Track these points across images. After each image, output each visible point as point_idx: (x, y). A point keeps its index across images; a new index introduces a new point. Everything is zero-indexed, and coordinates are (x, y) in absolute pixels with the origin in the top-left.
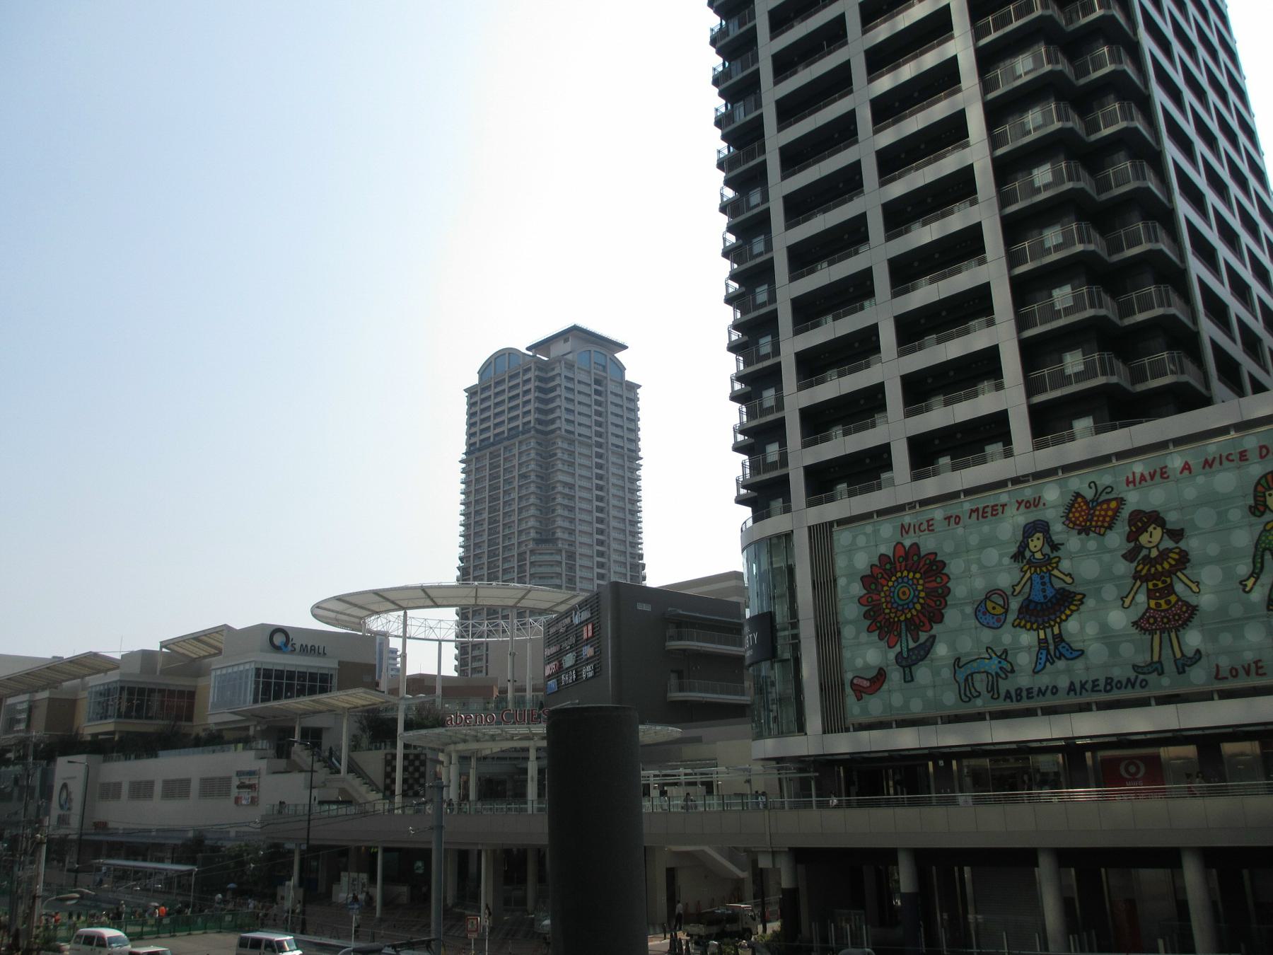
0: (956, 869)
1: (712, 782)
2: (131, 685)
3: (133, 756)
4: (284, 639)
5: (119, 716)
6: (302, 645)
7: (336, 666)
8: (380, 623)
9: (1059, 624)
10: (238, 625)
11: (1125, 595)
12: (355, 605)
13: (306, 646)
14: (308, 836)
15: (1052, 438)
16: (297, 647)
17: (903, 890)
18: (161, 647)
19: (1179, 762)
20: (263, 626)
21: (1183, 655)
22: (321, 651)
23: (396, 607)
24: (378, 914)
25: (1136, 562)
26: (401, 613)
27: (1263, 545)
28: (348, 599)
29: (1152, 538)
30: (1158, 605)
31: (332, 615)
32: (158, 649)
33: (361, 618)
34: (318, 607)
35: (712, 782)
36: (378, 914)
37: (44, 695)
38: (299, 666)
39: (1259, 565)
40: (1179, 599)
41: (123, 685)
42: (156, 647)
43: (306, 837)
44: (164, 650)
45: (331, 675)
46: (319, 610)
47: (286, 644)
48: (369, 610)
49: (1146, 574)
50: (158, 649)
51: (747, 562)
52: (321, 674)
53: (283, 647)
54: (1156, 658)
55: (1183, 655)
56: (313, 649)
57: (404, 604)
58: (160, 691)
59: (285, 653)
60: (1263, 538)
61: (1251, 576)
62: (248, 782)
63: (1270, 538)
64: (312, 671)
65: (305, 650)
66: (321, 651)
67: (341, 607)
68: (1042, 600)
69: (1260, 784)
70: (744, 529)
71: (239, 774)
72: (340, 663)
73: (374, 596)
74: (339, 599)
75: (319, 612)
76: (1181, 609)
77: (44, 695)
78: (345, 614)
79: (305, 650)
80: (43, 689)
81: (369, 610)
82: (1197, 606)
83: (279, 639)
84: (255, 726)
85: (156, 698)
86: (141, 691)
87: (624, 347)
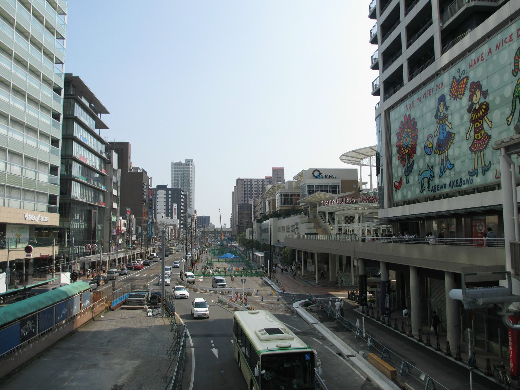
0: (425, 278)
2: (284, 193)
6: (326, 175)
8: (366, 161)
9: (447, 150)
10: (306, 170)
11: (467, 133)
12: (361, 154)
13: (328, 175)
15: (447, 47)
16: (324, 176)
18: (294, 179)
19: (491, 224)
20: (310, 169)
21: (485, 165)
22: (334, 177)
24: (317, 282)
25: (471, 113)
26: (369, 158)
27: (516, 94)
29: (477, 98)
30: (478, 136)
31: (349, 161)
32: (293, 180)
33: (358, 161)
34: (344, 155)
36: (317, 282)
38: (333, 183)
39: (514, 107)
40: (485, 133)
44: (295, 180)
45: (339, 186)
47: (319, 175)
48: (366, 155)
49: (474, 119)
50: (293, 180)
52: (334, 185)
53: (318, 177)
54: (476, 168)
55: (485, 165)
56: (330, 176)
57: (369, 154)
58: (295, 195)
59: (319, 179)
60: (516, 90)
61: (511, 114)
63: (519, 89)
64: (334, 184)
65: (327, 177)
66: (334, 177)
67: (354, 154)
68: (443, 139)
69: (462, 240)
72: (341, 181)
73: (370, 149)
74: (354, 151)
75: (343, 158)
76: (485, 138)
79: (327, 177)
81: (366, 155)
82: (491, 136)
83: (316, 174)
86: (288, 195)
87: (106, 112)
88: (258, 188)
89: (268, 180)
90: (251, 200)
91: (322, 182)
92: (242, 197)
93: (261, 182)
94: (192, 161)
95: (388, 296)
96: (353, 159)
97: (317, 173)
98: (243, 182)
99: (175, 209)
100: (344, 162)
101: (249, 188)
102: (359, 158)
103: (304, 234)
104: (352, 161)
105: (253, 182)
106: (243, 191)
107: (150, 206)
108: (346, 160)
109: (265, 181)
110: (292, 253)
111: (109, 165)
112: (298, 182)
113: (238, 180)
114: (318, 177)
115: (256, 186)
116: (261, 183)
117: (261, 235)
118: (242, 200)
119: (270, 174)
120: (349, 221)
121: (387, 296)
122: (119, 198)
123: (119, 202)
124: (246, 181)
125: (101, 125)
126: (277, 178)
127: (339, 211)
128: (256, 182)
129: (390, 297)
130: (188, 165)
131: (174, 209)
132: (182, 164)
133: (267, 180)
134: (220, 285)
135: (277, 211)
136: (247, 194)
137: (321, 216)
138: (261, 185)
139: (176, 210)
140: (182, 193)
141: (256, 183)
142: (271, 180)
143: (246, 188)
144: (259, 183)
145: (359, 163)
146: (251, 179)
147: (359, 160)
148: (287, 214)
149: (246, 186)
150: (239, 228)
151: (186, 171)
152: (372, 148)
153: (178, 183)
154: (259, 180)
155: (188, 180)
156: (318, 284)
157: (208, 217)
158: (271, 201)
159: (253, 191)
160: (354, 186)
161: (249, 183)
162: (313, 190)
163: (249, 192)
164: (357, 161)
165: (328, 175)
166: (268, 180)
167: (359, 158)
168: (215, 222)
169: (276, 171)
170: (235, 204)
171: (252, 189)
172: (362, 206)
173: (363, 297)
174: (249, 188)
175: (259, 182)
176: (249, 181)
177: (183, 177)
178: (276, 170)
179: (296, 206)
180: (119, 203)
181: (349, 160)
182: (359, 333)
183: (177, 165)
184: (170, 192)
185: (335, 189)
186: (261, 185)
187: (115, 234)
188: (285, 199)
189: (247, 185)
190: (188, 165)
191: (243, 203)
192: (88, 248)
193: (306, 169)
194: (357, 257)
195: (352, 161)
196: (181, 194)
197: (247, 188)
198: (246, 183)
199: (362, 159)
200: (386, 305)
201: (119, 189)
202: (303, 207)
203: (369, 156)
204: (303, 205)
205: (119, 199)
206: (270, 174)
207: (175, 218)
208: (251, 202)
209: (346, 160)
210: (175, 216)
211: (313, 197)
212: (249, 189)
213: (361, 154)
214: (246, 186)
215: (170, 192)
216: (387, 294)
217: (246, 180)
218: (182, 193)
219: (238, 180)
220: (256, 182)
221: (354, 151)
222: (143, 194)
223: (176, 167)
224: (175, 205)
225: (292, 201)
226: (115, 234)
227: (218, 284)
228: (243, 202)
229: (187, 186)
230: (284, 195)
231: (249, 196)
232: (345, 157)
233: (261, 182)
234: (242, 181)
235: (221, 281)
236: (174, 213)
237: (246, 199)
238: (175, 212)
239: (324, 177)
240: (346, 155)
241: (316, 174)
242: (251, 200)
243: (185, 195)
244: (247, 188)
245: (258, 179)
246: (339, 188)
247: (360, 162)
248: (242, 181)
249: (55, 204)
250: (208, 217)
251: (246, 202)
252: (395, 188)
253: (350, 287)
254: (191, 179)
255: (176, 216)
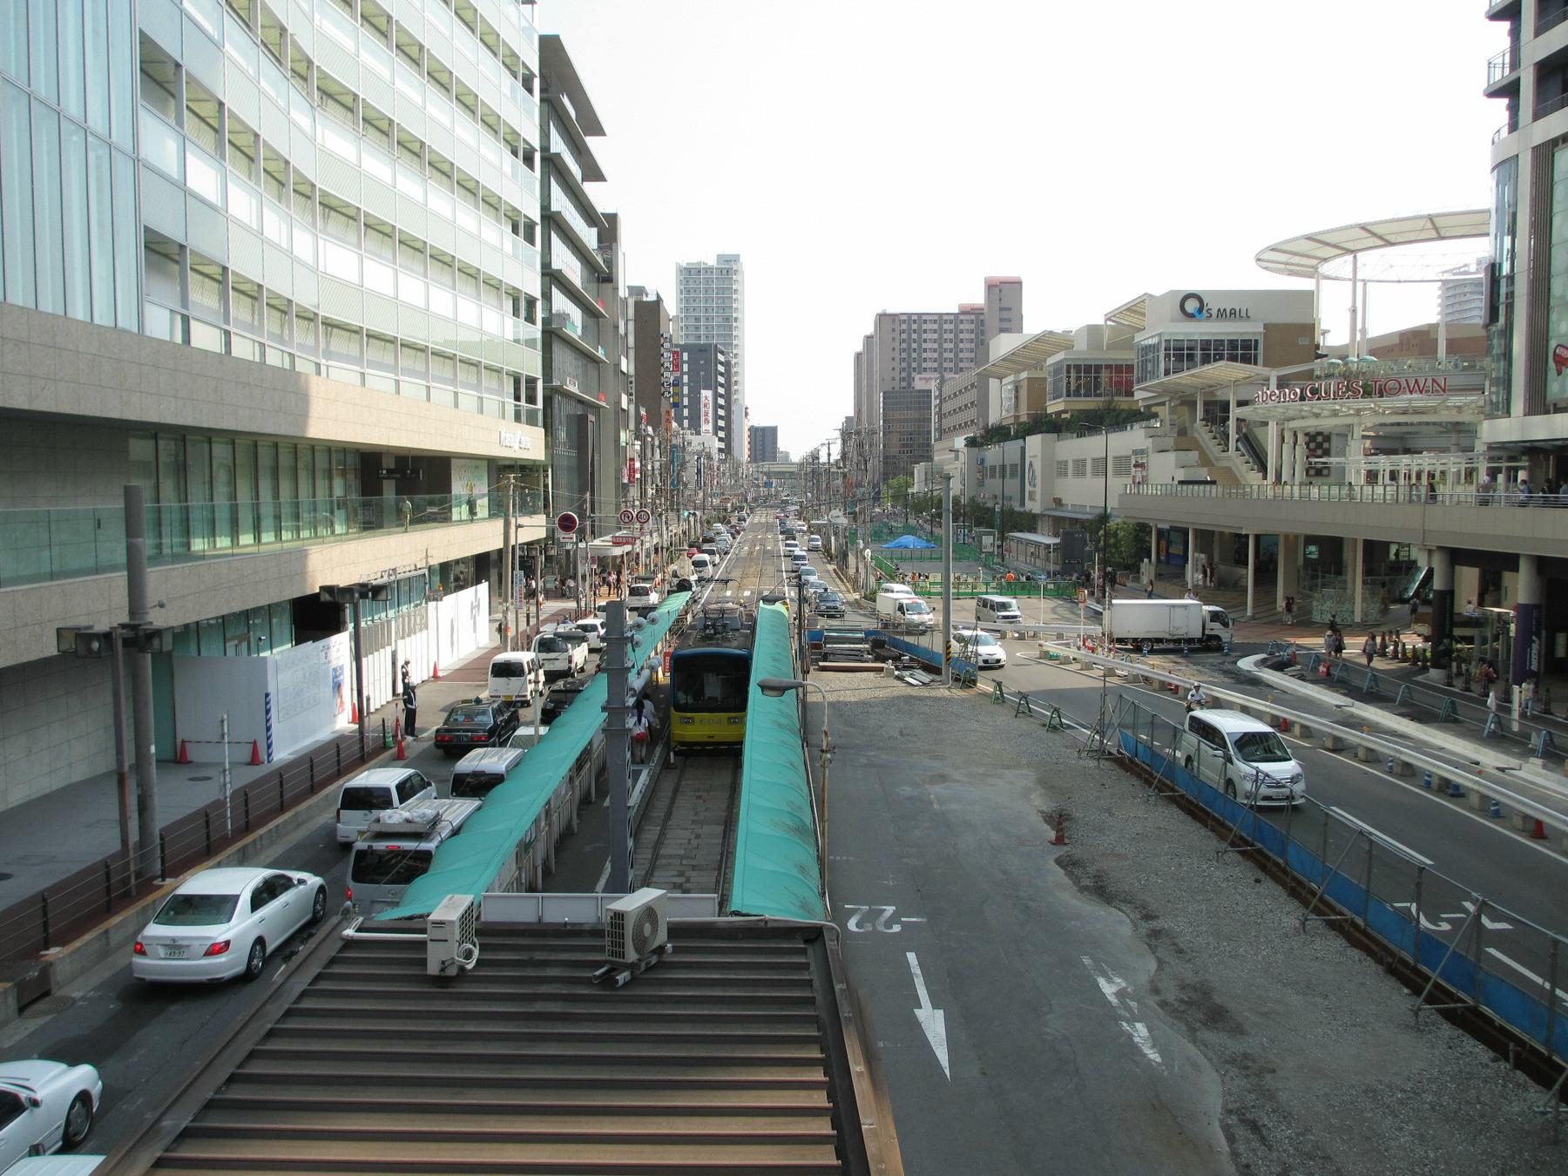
1: (1378, 471)
3: (1075, 435)
4: (1197, 305)
5: (1068, 395)
6: (1219, 310)
7: (1262, 330)
12: (1328, 244)
13: (1225, 310)
14: (234, 448)
16: (1214, 312)
17: (1435, 587)
18: (1106, 320)
20: (1172, 293)
23: (1383, 243)
24: (1249, 612)
26: (1350, 258)
28: (1318, 237)
31: (1282, 266)
35: (1378, 471)
36: (1249, 612)
37: (1024, 375)
41: (1069, 363)
42: (1100, 321)
43: (213, 445)
44: (1109, 323)
45: (1256, 341)
46: (1265, 260)
47: (1200, 310)
48: (1342, 248)
51: (1497, 186)
53: (1196, 314)
56: (1233, 313)
57: (1351, 246)
58: (1108, 367)
59: (1199, 321)
62: (1136, 463)
65: (1222, 314)
70: (1496, 140)
71: (1135, 452)
72: (1266, 326)
77: (1024, 375)
78: (1308, 257)
79: (1222, 314)
80: (1023, 371)
83: (1191, 306)
84: (1170, 401)
85: (1104, 374)
86: (1088, 368)
88: (940, 341)
89: (973, 317)
90: (920, 379)
91: (1221, 331)
92: (893, 369)
93: (951, 322)
94: (735, 259)
95: (1538, 642)
96: (1296, 260)
97: (1192, 305)
98: (897, 321)
99: (705, 406)
100: (1266, 268)
101: (915, 341)
102: (1314, 257)
103: (1176, 482)
104: (1292, 264)
105: (925, 322)
106: (897, 350)
107: (676, 401)
108: (1273, 262)
109: (962, 322)
110: (1136, 536)
111: (610, 285)
112: (1118, 329)
113: (883, 318)
114: (1196, 314)
115: (936, 336)
116: (952, 327)
117: (981, 483)
118: (894, 379)
119: (978, 298)
120: (1312, 445)
121: (1534, 641)
122: (633, 379)
123: (633, 391)
124: (904, 321)
125: (594, 173)
126: (1001, 309)
127: (1303, 418)
128: (935, 322)
129: (1540, 645)
130: (724, 272)
131: (702, 406)
132: (709, 270)
133: (968, 317)
134: (1005, 617)
135: (1051, 414)
136: (908, 360)
137: (1211, 431)
138: (951, 331)
139: (707, 409)
140: (721, 358)
141: (936, 327)
142: (982, 317)
143: (904, 341)
144: (946, 326)
145: (1312, 273)
146: (920, 315)
147: (1316, 262)
148: (1089, 424)
149: (904, 336)
150: (886, 463)
151: (721, 290)
152: (1368, 227)
153: (697, 328)
154: (945, 318)
155: (727, 319)
156: (1253, 618)
157: (774, 430)
158: (1025, 384)
159: (925, 350)
160: (1303, 341)
161: (914, 327)
162: (1183, 354)
163: (914, 355)
164: (1308, 266)
165: (1225, 310)
166: (973, 317)
167: (1314, 257)
168: (794, 446)
169: (997, 290)
170: (870, 386)
171: (924, 346)
172: (1379, 407)
173: (1442, 647)
174: (915, 341)
175: (946, 322)
176: (915, 321)
177: (710, 310)
178: (996, 286)
179: (1116, 399)
180: (631, 394)
181: (1283, 263)
182: (1495, 723)
183: (692, 272)
184: (685, 356)
185: (1242, 351)
186: (951, 331)
187: (626, 481)
188: (1078, 378)
189: (909, 331)
190: (724, 272)
191: (897, 389)
192: (627, 520)
193: (1158, 291)
194: (1433, 544)
195: (1292, 264)
196: (718, 362)
197: (909, 340)
198: (904, 327)
199: (1325, 260)
200: (1531, 665)
201: (632, 353)
202: (1140, 404)
203: (1352, 252)
204: (1142, 399)
205: (631, 383)
206: (978, 298)
207: (707, 431)
208: (923, 382)
209: (1273, 262)
210: (707, 427)
211: (1197, 377)
212: (914, 346)
213: (1328, 244)
214: (904, 336)
215: (685, 356)
216: (1534, 638)
217: (905, 317)
218: (721, 358)
219: (883, 318)
220: (935, 322)
221: (1309, 238)
222: (663, 365)
223: (691, 276)
224: (707, 395)
225: (1097, 386)
226: (626, 481)
227: (999, 614)
228: (896, 384)
229: (724, 336)
230: (1078, 368)
231: (914, 365)
232: (1280, 256)
233: (951, 322)
234: (894, 321)
235: (1004, 606)
236: (703, 418)
237: (904, 375)
238: (706, 414)
239: (1214, 315)
240: (1279, 247)
241: (1191, 306)
242: (920, 379)
243: (727, 365)
244: (909, 340)
245: (940, 315)
246: (1256, 349)
247: (1315, 268)
248: (894, 321)
249: (535, 403)
250: (774, 430)
251: (904, 384)
252: (1556, 362)
253: (1350, 626)
254: (734, 315)
255: (710, 427)
